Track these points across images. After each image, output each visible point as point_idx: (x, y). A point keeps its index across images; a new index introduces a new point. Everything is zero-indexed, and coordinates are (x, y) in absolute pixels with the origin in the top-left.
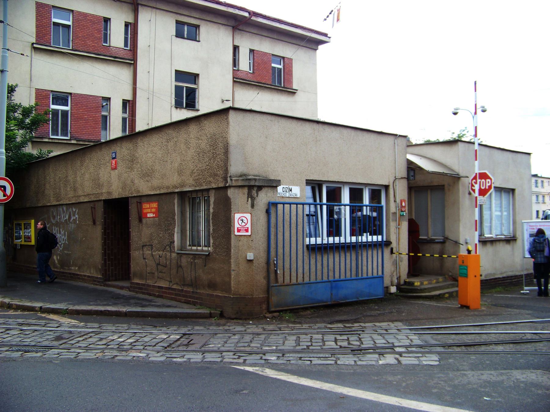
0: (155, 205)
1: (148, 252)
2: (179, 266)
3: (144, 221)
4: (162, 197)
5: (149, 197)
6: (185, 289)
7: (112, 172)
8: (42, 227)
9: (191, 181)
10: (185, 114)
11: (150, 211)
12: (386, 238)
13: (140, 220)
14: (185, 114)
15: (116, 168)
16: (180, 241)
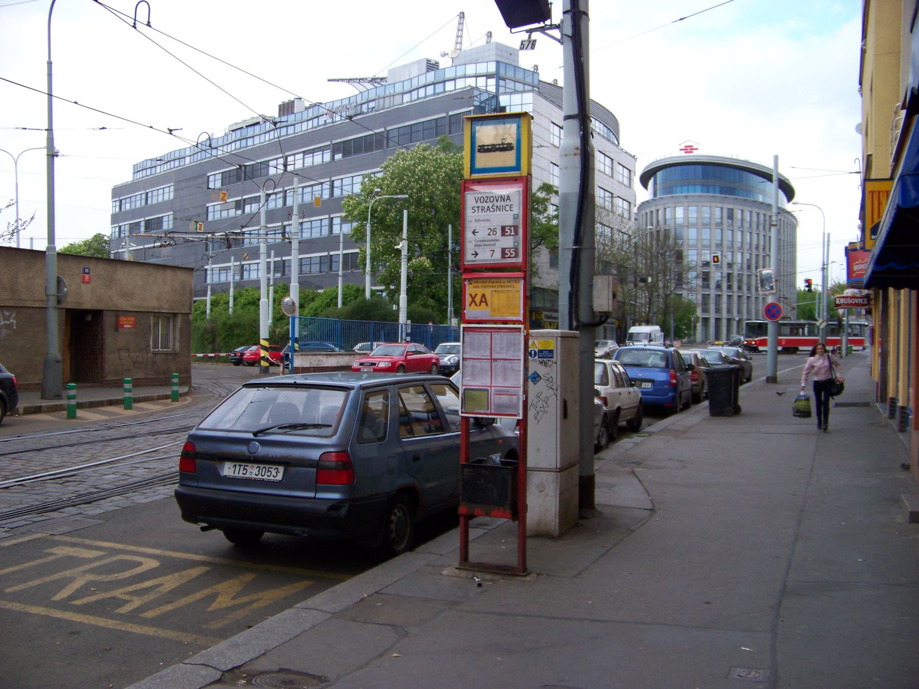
0: (132, 319)
1: (124, 354)
2: (154, 363)
3: (120, 330)
4: (140, 314)
5: (127, 313)
6: (160, 376)
7: (84, 286)
8: (281, 469)
9: (167, 306)
10: (477, 148)
11: (127, 324)
12: (899, 294)
13: (117, 330)
14: (477, 148)
15: (89, 283)
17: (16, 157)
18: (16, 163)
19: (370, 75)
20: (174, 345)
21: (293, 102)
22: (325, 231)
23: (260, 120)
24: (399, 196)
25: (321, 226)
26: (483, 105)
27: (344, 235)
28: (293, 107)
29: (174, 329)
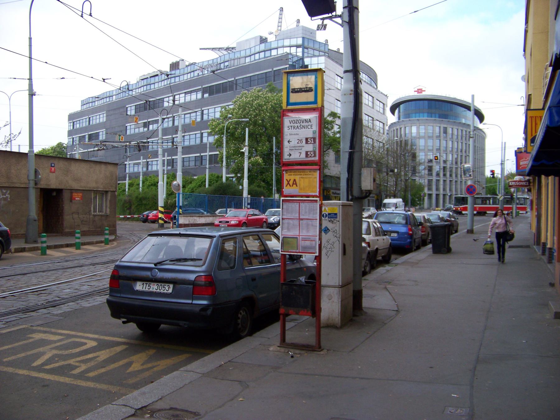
0: (81, 194)
1: (76, 216)
2: (94, 221)
3: (73, 201)
4: (85, 192)
5: (77, 191)
6: (97, 229)
7: (51, 174)
9: (102, 187)
10: (291, 90)
11: (78, 197)
13: (71, 201)
14: (291, 90)
15: (54, 172)
16: (355, 17)
17: (9, 96)
18: (10, 99)
19: (225, 46)
20: (106, 210)
21: (178, 62)
22: (198, 141)
23: (159, 73)
24: (243, 120)
25: (196, 138)
26: (294, 64)
27: (210, 143)
28: (178, 65)
29: (106, 200)
